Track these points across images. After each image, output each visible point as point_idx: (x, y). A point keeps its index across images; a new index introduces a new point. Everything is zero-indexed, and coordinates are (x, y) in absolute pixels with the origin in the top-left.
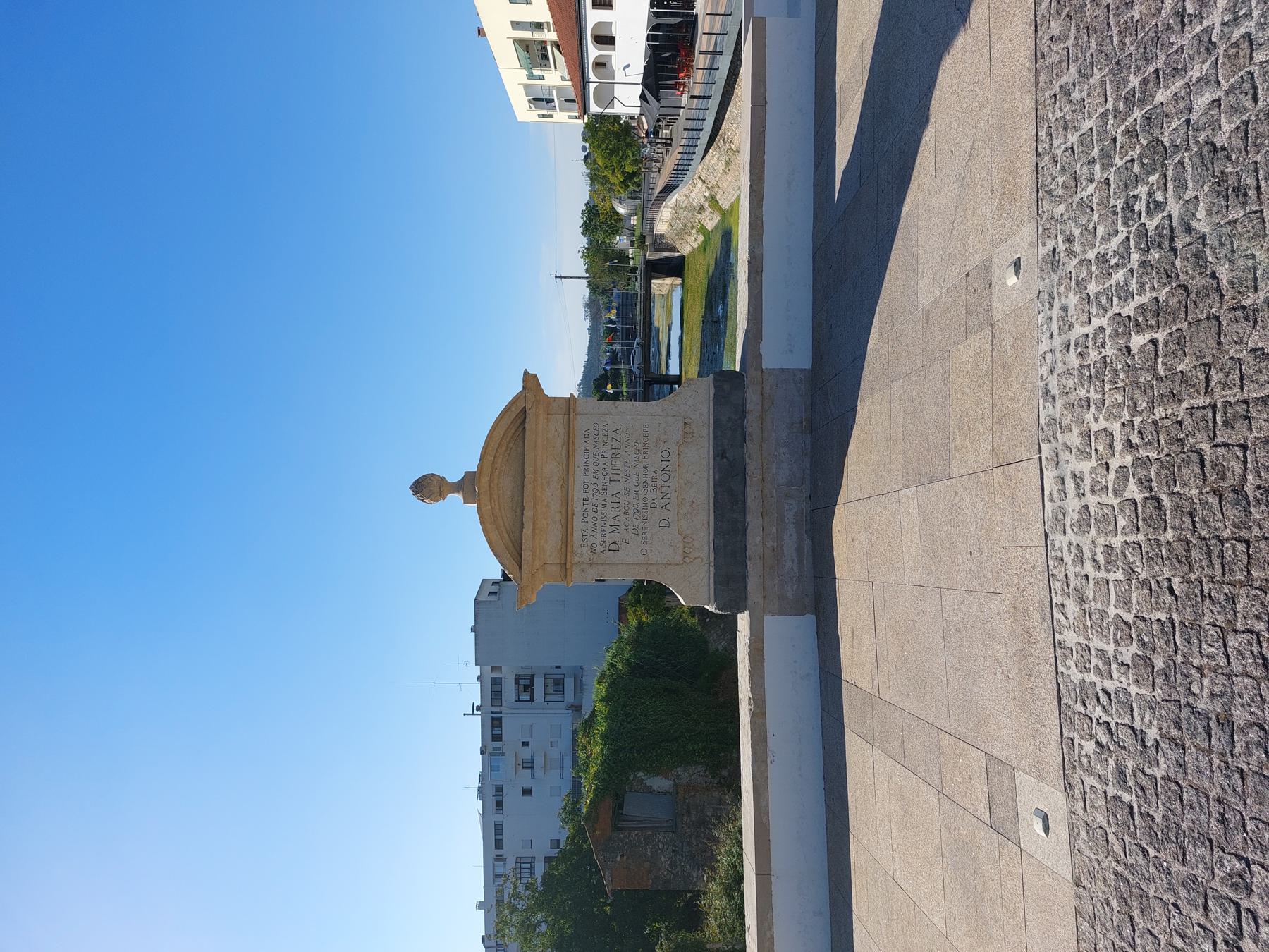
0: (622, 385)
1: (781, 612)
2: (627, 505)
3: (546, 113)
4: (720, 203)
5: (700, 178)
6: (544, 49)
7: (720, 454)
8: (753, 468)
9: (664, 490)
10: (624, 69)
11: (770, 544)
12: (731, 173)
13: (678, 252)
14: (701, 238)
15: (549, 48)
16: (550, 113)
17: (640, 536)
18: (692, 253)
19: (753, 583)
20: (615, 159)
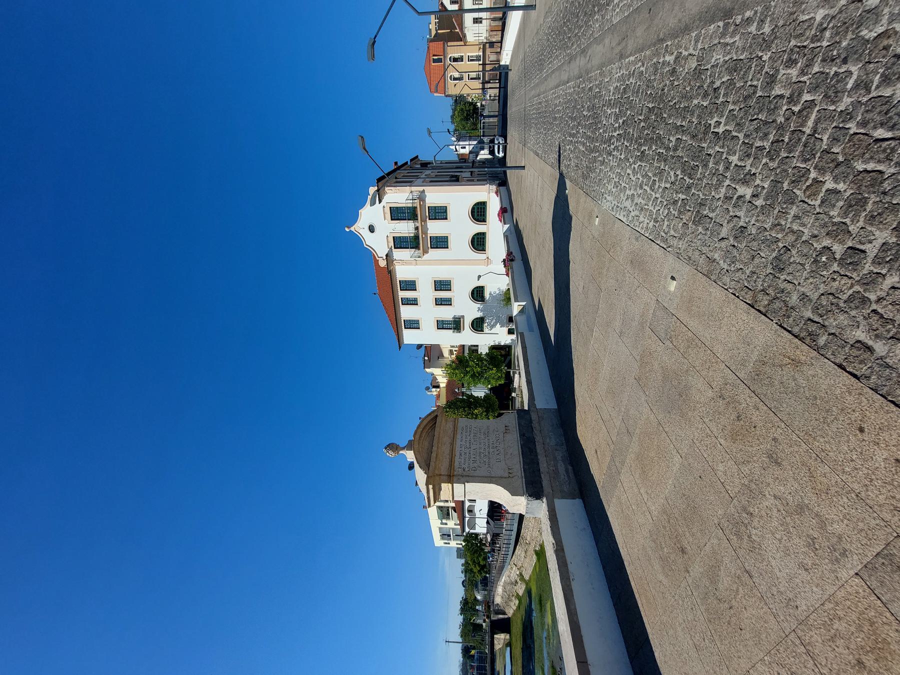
0: (477, 658)
1: (563, 498)
2: (480, 453)
3: (447, 542)
4: (525, 576)
5: (514, 564)
6: (448, 510)
7: (522, 435)
8: (538, 439)
9: (497, 448)
10: (480, 511)
11: (551, 468)
12: (528, 557)
13: (507, 615)
14: (517, 602)
15: (450, 509)
16: (449, 542)
17: (487, 465)
18: (514, 614)
19: (545, 483)
20: (476, 555)
